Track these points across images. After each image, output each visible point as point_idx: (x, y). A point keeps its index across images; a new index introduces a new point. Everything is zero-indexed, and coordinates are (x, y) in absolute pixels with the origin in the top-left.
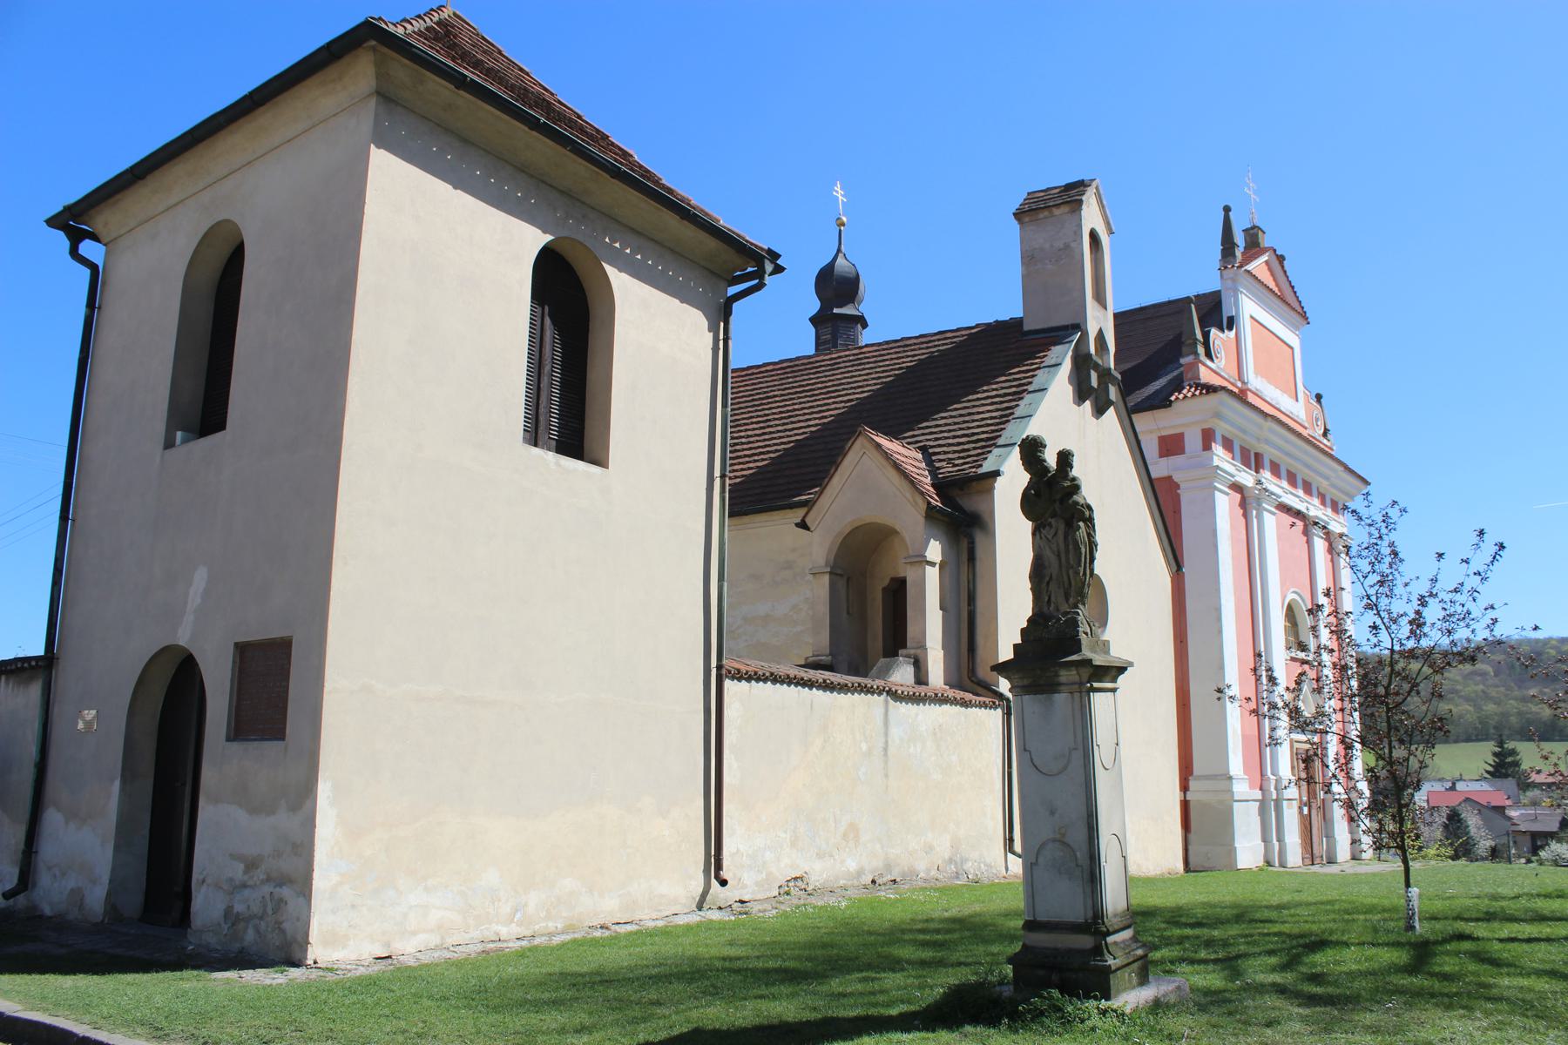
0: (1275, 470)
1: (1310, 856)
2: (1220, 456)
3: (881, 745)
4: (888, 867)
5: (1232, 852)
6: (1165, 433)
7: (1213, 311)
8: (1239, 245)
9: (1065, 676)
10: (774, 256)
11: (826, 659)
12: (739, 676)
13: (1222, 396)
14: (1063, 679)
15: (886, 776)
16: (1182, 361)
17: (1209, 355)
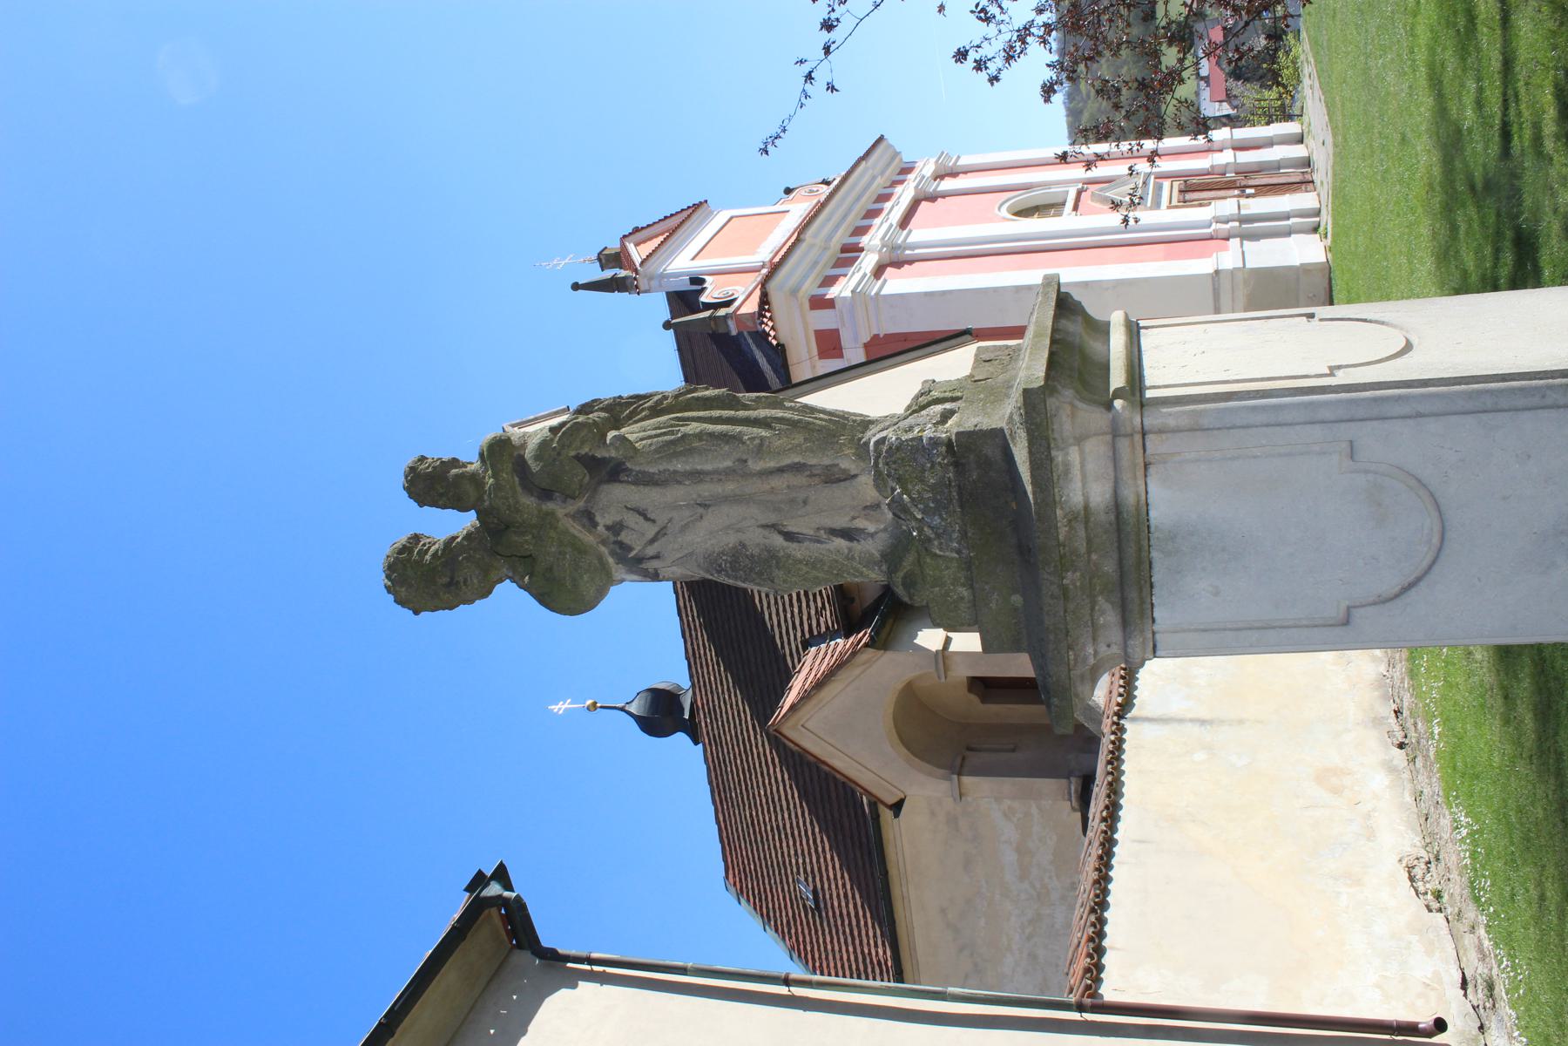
0: (861, 231)
1: (1305, 184)
2: (841, 290)
3: (1195, 729)
4: (1377, 722)
5: (1306, 269)
6: (815, 351)
7: (685, 299)
8: (616, 275)
9: (1086, 481)
10: (479, 881)
11: (1075, 785)
12: (1095, 971)
13: (772, 286)
14: (1099, 494)
15: (1241, 722)
16: (734, 332)
17: (728, 304)
